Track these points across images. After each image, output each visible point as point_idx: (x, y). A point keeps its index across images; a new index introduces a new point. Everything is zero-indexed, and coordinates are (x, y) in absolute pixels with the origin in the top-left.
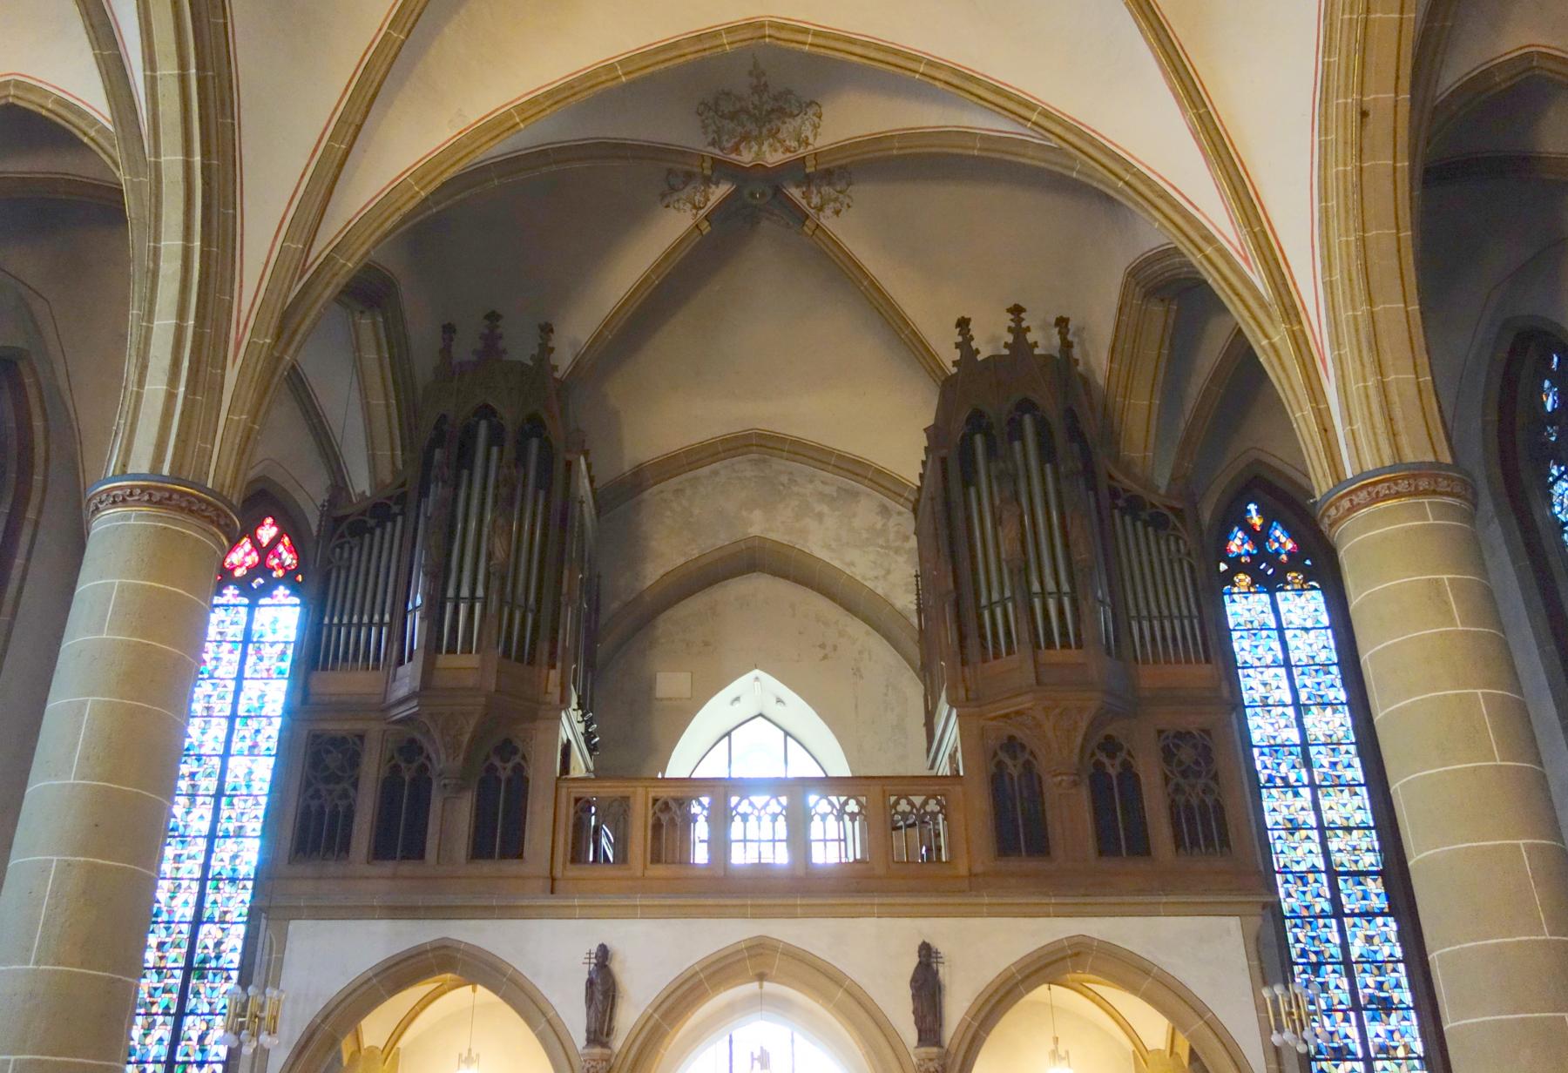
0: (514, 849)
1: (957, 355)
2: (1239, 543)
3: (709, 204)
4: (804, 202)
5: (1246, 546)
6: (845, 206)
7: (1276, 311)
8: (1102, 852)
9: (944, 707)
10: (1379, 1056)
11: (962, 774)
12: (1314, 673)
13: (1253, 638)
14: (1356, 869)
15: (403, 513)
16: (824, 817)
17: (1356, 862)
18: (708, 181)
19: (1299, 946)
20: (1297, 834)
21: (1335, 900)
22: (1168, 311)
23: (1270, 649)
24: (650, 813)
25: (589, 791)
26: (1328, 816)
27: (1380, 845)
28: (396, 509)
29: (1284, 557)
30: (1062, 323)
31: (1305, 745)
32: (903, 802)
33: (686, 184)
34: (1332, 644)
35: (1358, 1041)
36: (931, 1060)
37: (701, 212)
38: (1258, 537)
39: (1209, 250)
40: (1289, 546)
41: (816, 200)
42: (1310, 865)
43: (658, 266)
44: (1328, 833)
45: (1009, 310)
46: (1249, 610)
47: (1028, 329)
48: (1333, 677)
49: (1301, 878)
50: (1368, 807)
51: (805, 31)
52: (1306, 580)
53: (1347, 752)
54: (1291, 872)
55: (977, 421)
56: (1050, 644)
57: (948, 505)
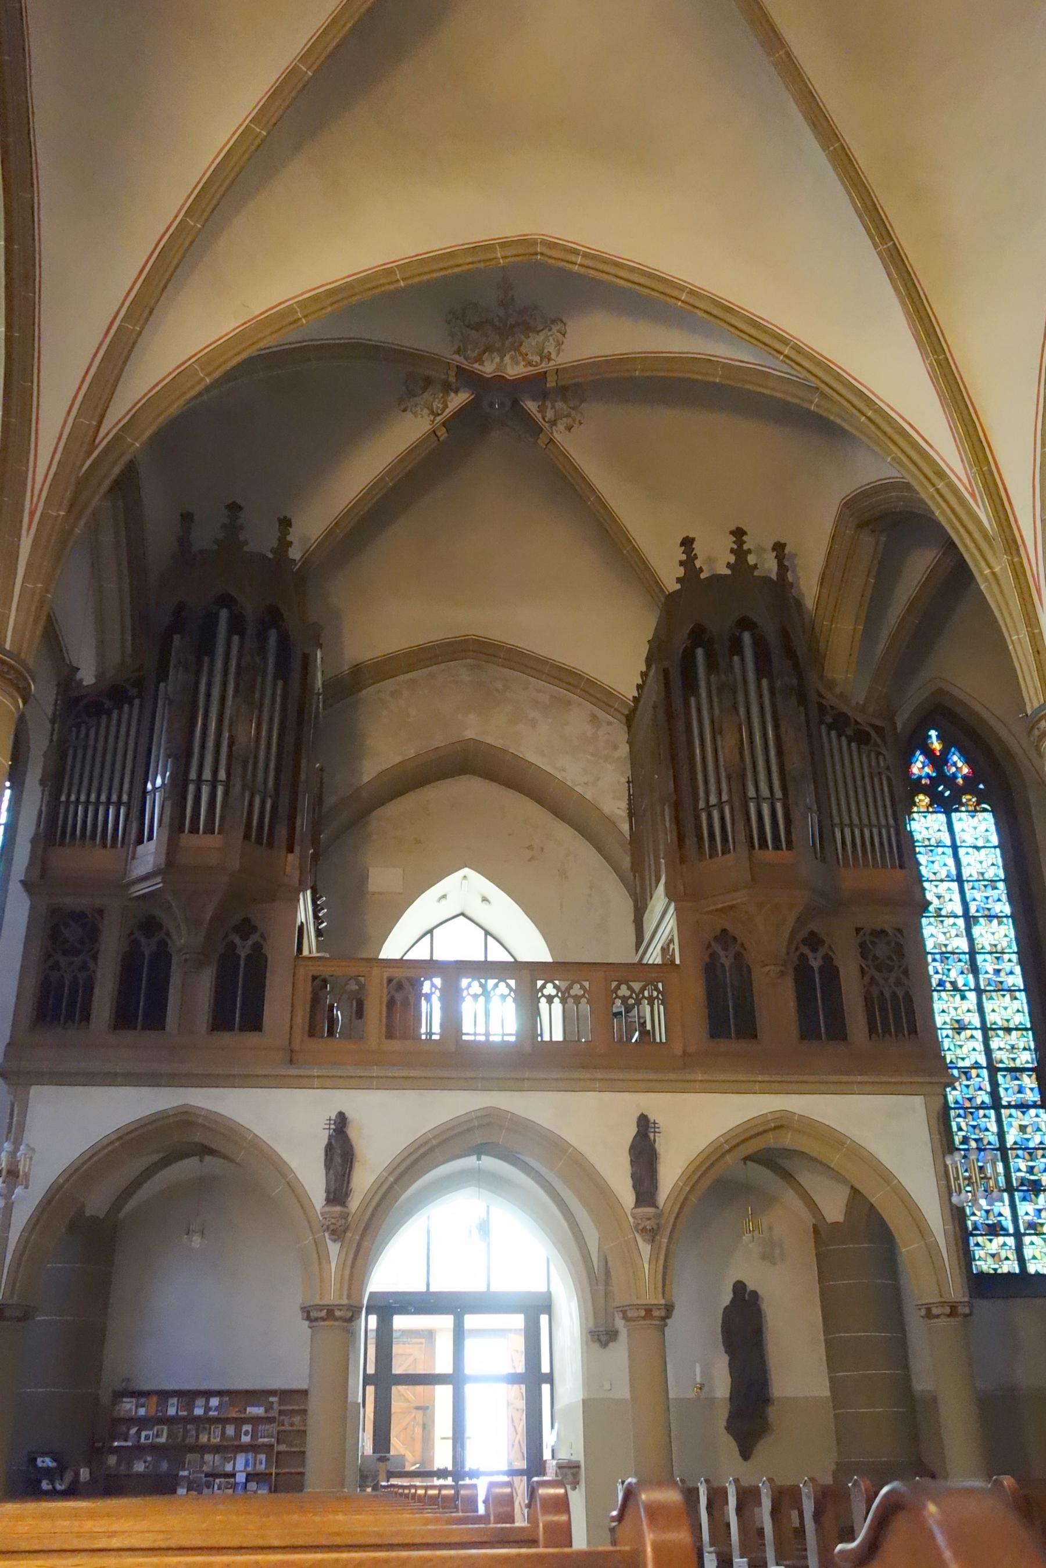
0: (254, 1022)
1: (681, 572)
2: (921, 766)
3: (447, 411)
4: (539, 416)
5: (927, 770)
6: (577, 422)
7: (999, 544)
8: (803, 1037)
9: (659, 900)
10: (1028, 1232)
11: (678, 962)
12: (983, 888)
13: (930, 854)
14: (1014, 1066)
15: (140, 696)
16: (550, 999)
17: (1014, 1059)
18: (447, 388)
19: (961, 1134)
20: (963, 1034)
21: (994, 1094)
22: (877, 543)
23: (945, 865)
24: (385, 991)
25: (325, 971)
26: (990, 1018)
27: (1036, 1045)
28: (133, 692)
29: (960, 781)
30: (779, 548)
31: (973, 953)
32: (624, 987)
33: (424, 390)
34: (1000, 863)
35: (1009, 1218)
36: (649, 1219)
37: (438, 418)
38: (938, 761)
39: (941, 485)
40: (966, 770)
41: (550, 414)
42: (973, 1061)
43: (390, 471)
44: (991, 1033)
45: (732, 533)
46: (927, 828)
47: (749, 551)
48: (1000, 892)
49: (965, 1073)
50: (1026, 1010)
51: (576, 252)
52: (978, 803)
53: (1010, 961)
54: (956, 1068)
55: (699, 636)
56: (763, 844)
57: (670, 715)
